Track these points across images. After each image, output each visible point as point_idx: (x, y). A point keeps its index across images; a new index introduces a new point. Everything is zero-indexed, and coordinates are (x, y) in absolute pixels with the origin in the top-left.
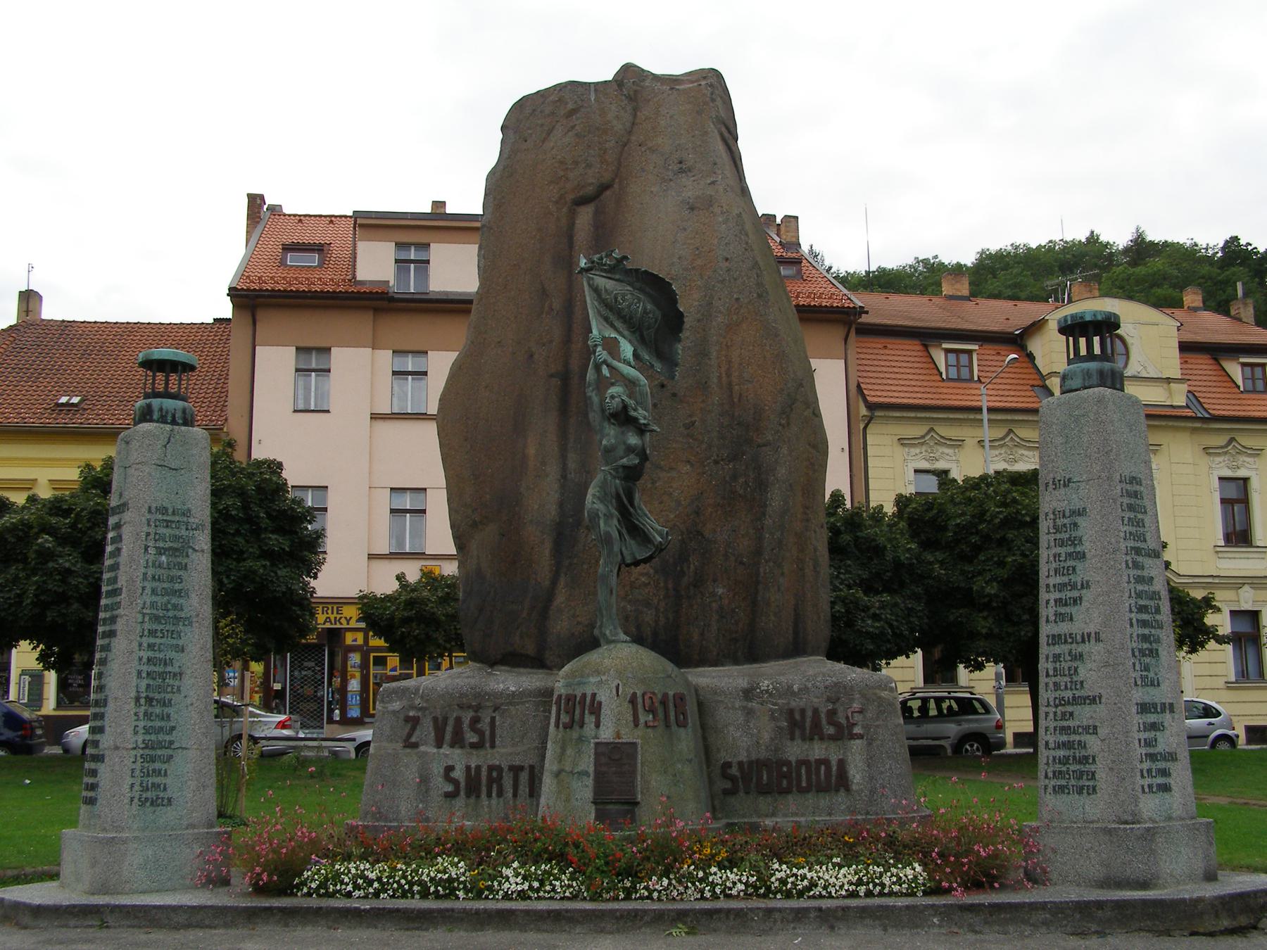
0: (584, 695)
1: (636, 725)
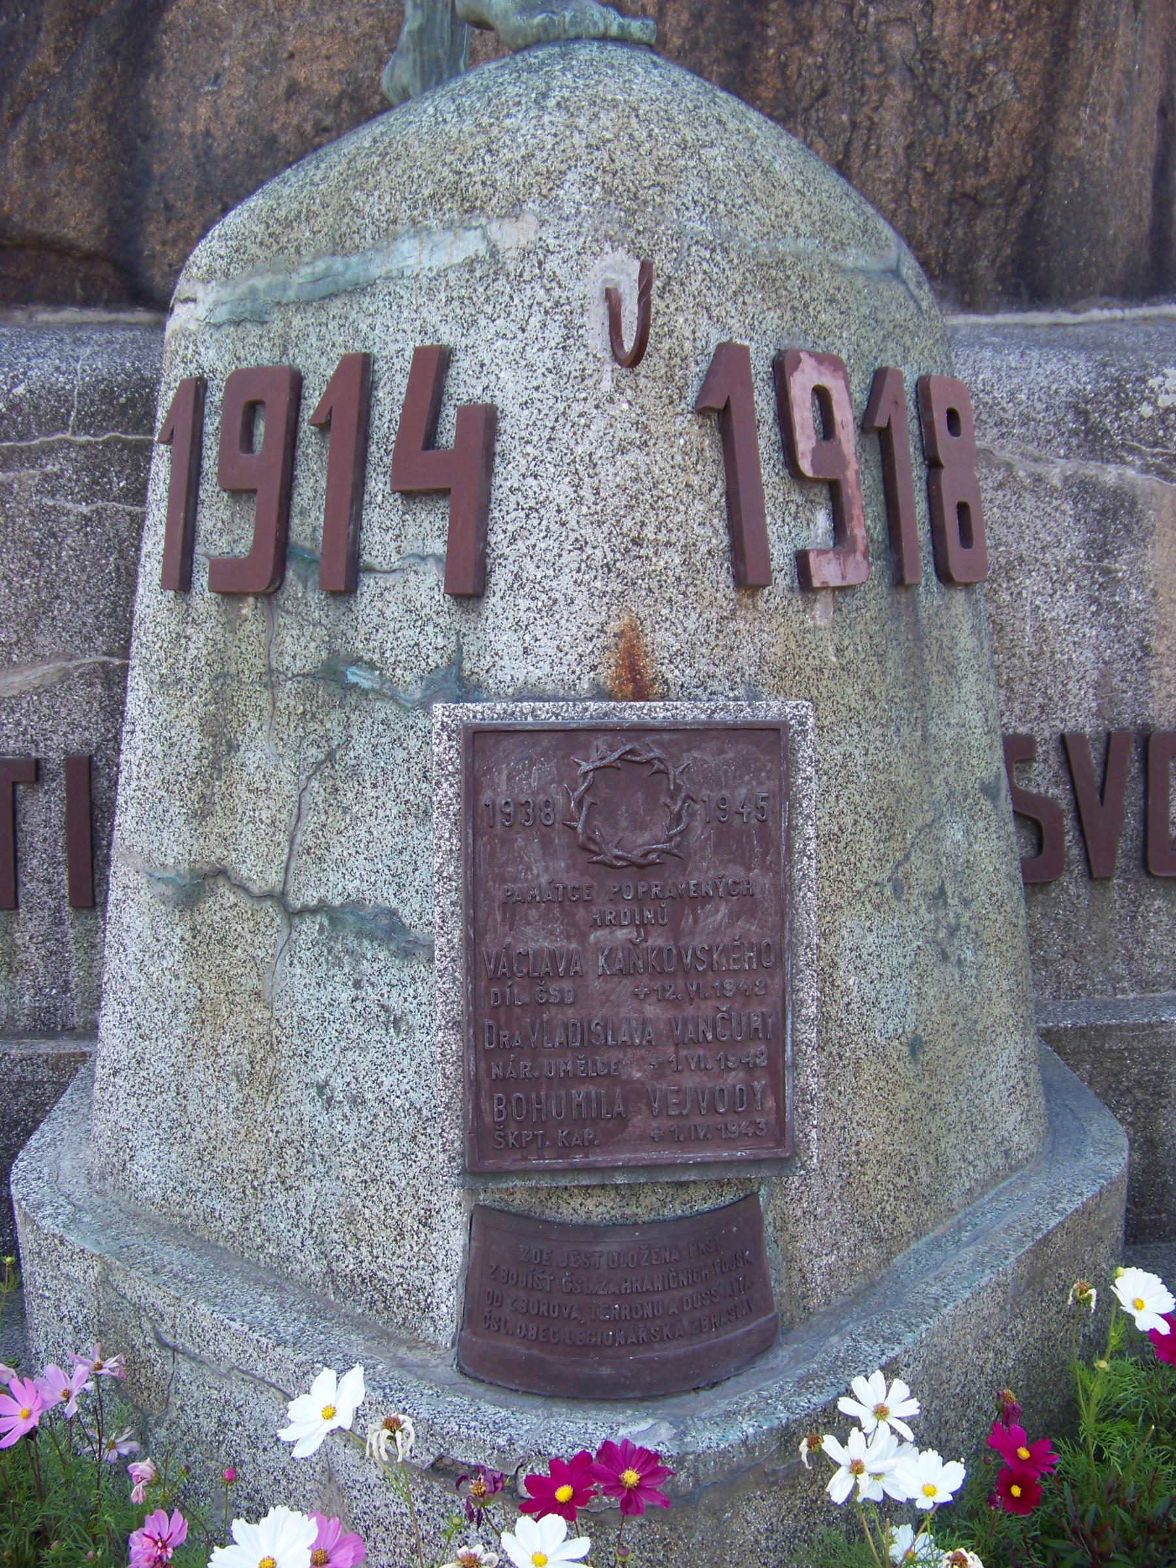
0: (360, 373)
1: (746, 568)
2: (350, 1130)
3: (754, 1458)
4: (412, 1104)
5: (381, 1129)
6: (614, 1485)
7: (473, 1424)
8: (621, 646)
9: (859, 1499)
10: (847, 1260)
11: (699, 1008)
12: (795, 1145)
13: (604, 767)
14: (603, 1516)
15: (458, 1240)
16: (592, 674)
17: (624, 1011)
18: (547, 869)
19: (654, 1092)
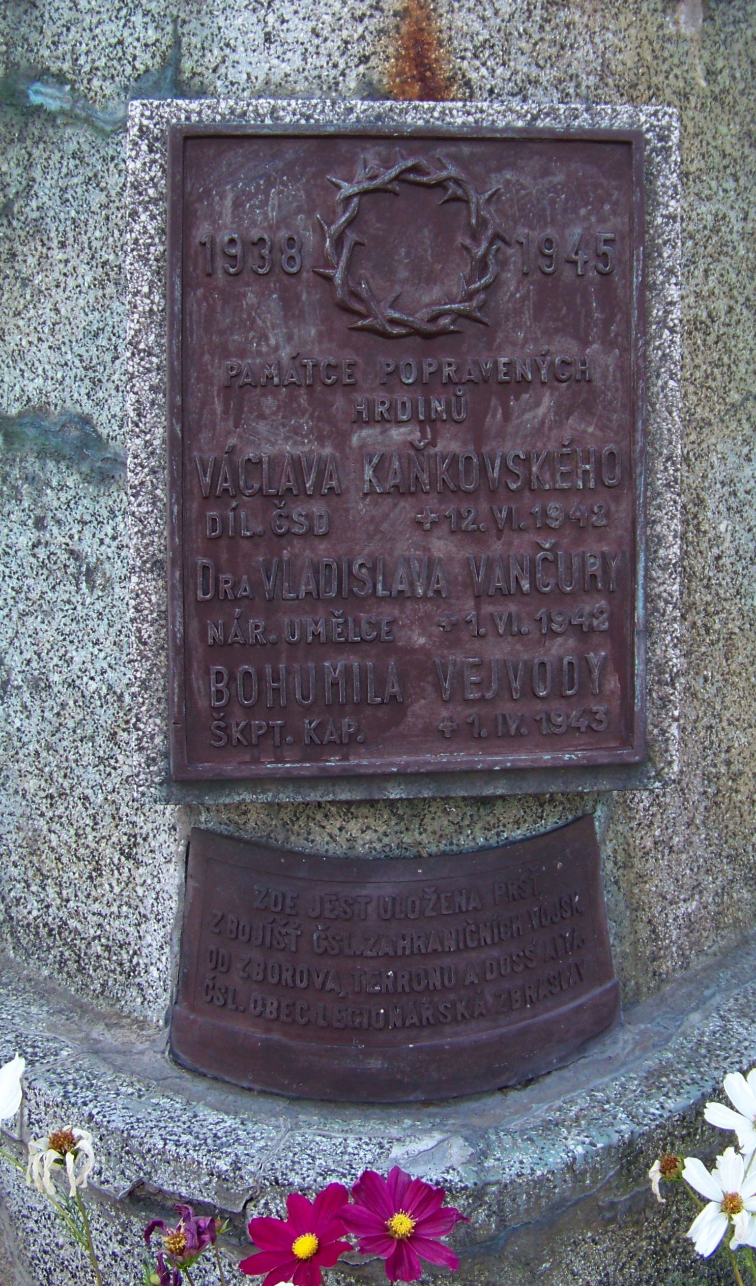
2: (32, 726)
3: (584, 1188)
4: (110, 688)
5: (71, 724)
6: (379, 1236)
7: (184, 1138)
8: (404, 29)
9: (733, 1245)
10: (712, 908)
11: (510, 544)
12: (648, 746)
13: (375, 191)
14: (368, 1271)
15: (172, 877)
16: (362, 69)
17: (402, 548)
18: (289, 338)
19: (444, 665)
